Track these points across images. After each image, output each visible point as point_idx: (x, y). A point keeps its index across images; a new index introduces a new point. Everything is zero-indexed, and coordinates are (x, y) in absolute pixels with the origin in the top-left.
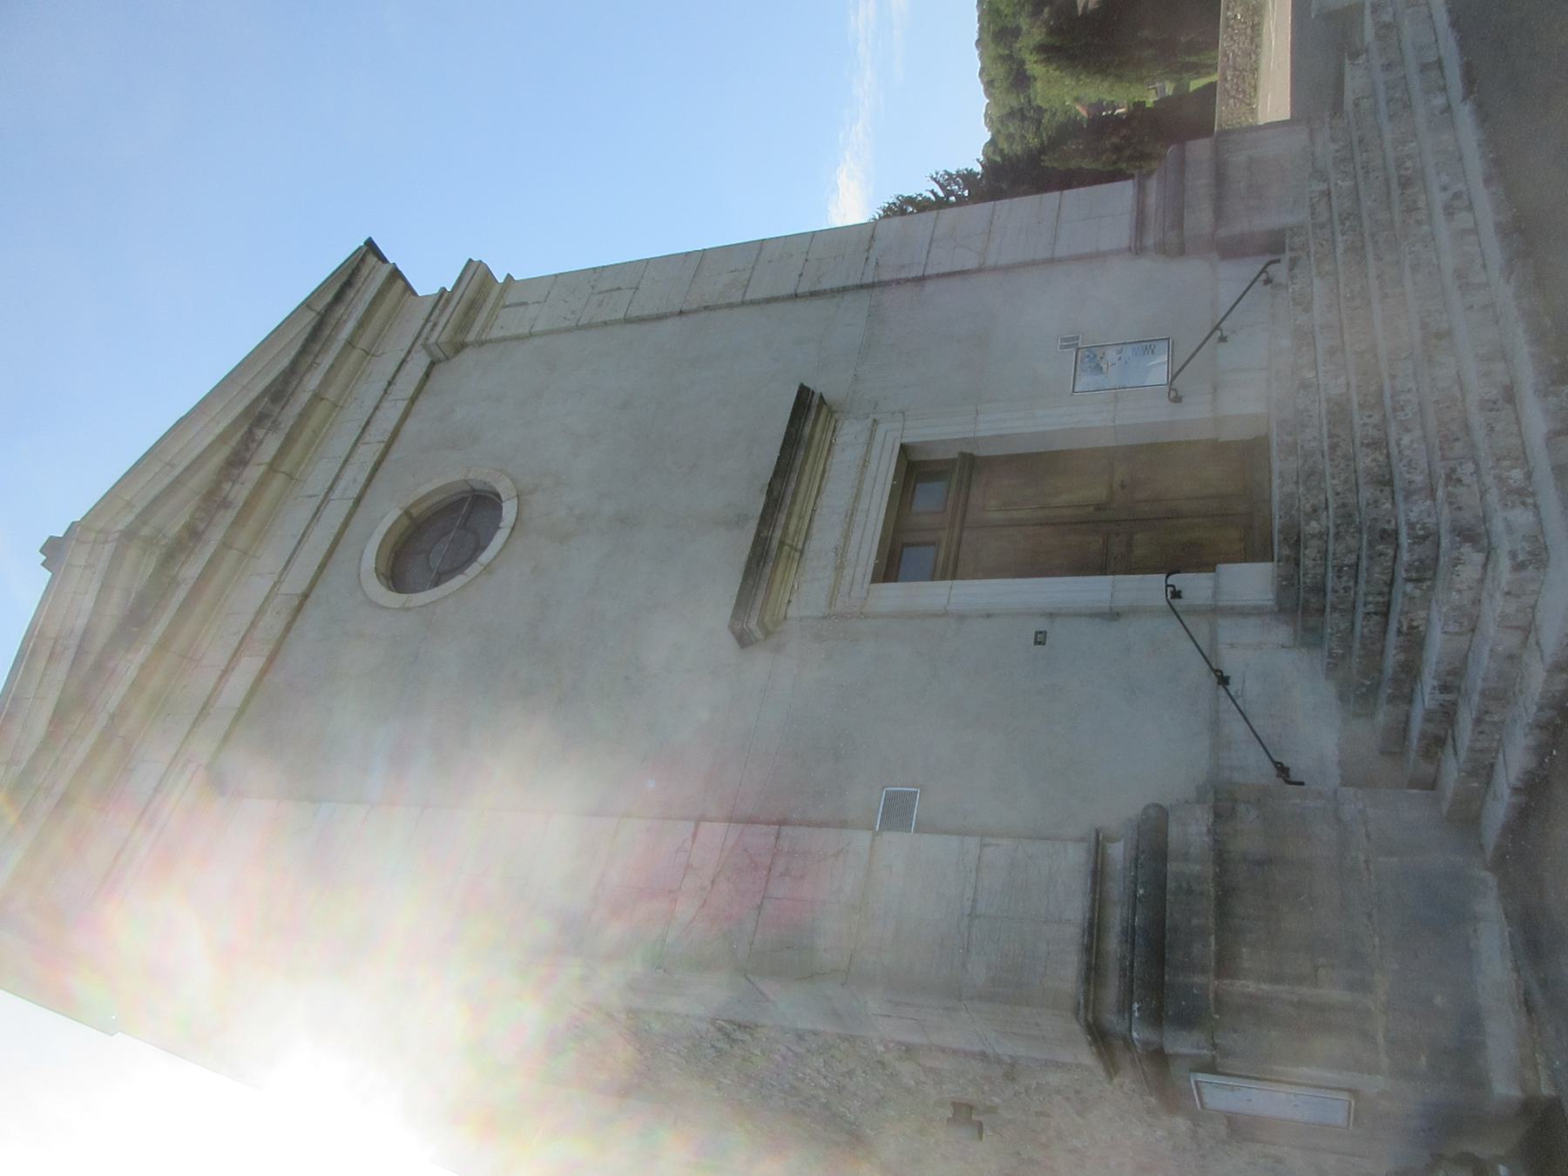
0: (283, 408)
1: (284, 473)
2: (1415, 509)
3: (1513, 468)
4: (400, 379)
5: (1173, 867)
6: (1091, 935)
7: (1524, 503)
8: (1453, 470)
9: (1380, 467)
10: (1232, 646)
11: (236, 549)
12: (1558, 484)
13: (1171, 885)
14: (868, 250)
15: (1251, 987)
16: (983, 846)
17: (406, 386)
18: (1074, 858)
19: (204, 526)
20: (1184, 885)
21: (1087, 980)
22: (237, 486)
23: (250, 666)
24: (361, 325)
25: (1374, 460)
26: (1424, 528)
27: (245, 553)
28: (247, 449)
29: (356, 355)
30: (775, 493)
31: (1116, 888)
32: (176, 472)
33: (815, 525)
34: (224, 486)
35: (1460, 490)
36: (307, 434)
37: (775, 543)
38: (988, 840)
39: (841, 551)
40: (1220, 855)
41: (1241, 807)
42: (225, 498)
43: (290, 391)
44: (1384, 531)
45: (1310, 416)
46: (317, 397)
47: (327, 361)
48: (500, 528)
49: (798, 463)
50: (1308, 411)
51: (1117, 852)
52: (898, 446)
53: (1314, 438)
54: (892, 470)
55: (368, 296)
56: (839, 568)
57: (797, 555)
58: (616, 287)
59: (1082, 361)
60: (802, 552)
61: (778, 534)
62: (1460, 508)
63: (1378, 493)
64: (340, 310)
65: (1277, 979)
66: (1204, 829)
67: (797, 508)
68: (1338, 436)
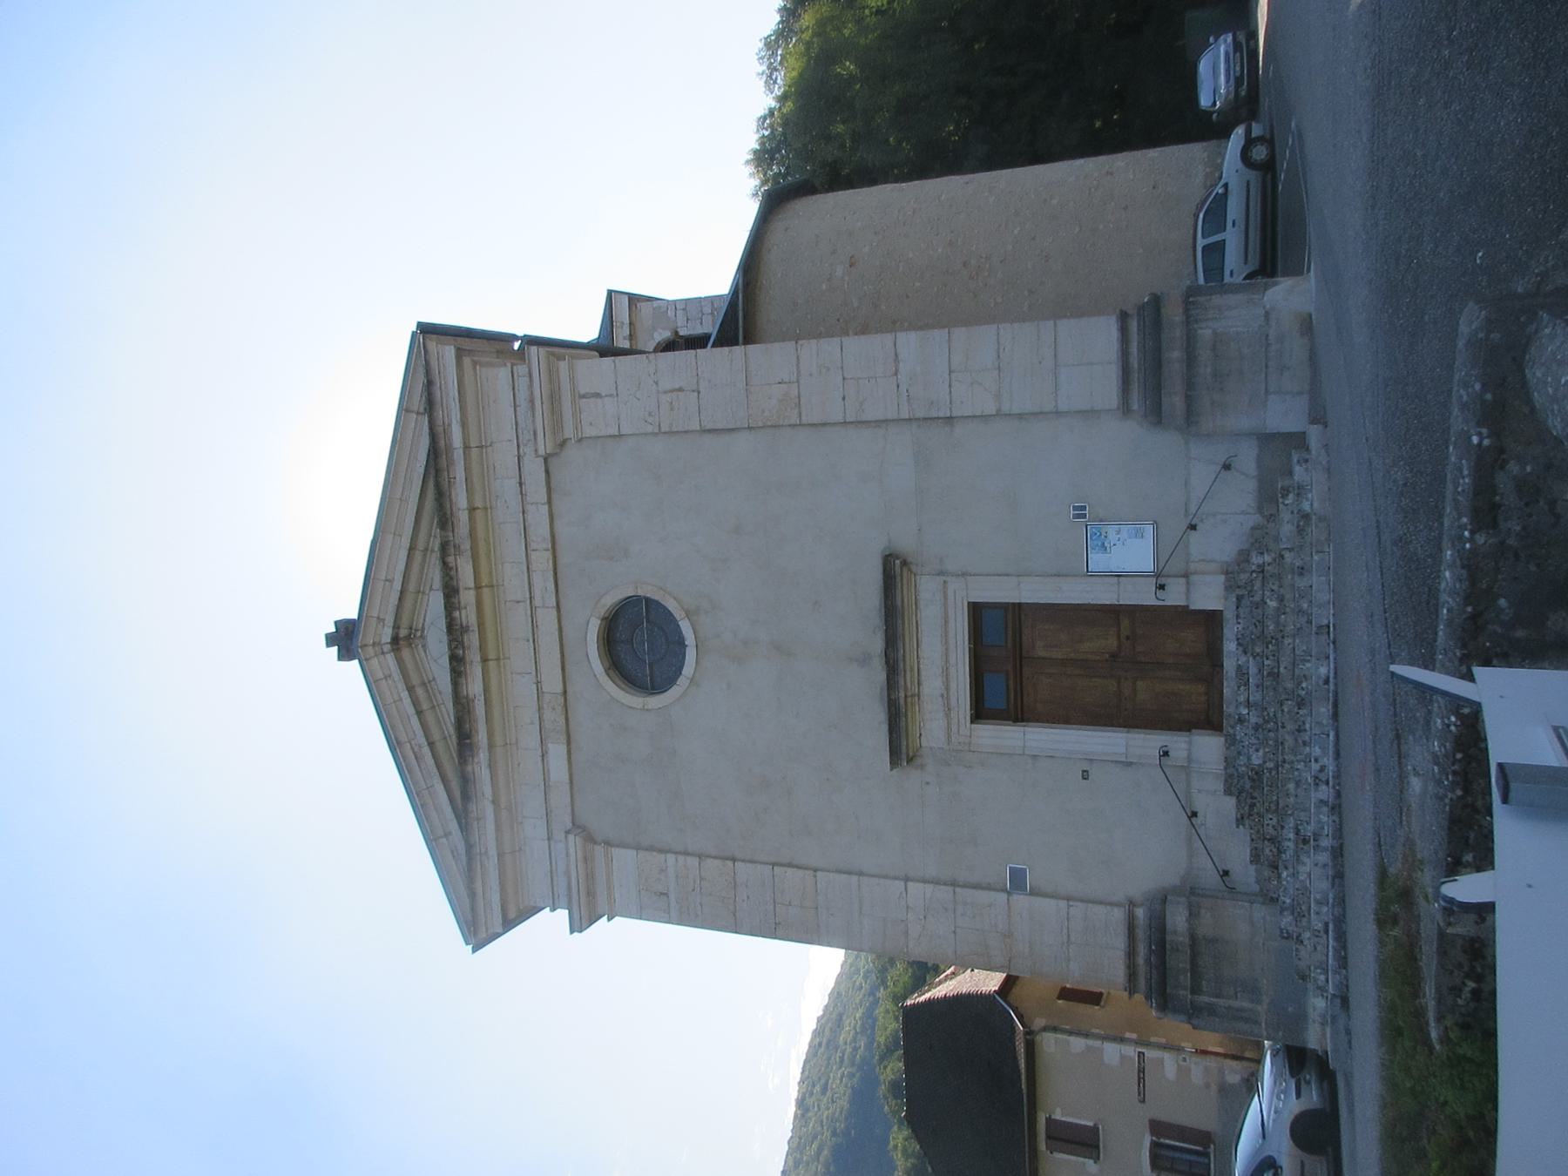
0: (453, 531)
1: (486, 586)
2: (1284, 920)
3: (1321, 974)
4: (527, 478)
5: (1168, 938)
6: (1129, 959)
7: (1322, 995)
8: (1300, 934)
9: (1274, 856)
10: (1199, 791)
11: (492, 660)
12: (1398, 659)
13: (1168, 946)
14: (896, 374)
15: (1206, 999)
16: (1069, 906)
17: (537, 491)
18: (1118, 915)
19: (461, 652)
20: (1175, 947)
21: (1130, 980)
22: (463, 612)
23: (557, 751)
24: (464, 424)
25: (1271, 851)
26: (1287, 932)
27: (498, 659)
28: (451, 578)
29: (492, 664)
30: (891, 661)
31: (1141, 934)
32: (398, 586)
33: (923, 673)
34: (454, 615)
35: (1301, 948)
36: (482, 544)
37: (902, 701)
38: (1071, 903)
39: (946, 697)
40: (1193, 938)
41: (1203, 911)
42: (461, 625)
43: (449, 512)
44: (1272, 898)
45: (1243, 746)
46: (472, 510)
47: (459, 473)
48: (686, 646)
49: (900, 629)
50: (1242, 742)
51: (1140, 912)
52: (966, 604)
53: (1245, 764)
54: (967, 638)
55: (453, 392)
56: (948, 715)
57: (917, 699)
58: (677, 386)
59: (1091, 538)
60: (919, 696)
61: (902, 694)
62: (1300, 959)
63: (1270, 872)
64: (439, 414)
65: (1218, 996)
66: (1184, 919)
67: (908, 668)
68: (1256, 798)
